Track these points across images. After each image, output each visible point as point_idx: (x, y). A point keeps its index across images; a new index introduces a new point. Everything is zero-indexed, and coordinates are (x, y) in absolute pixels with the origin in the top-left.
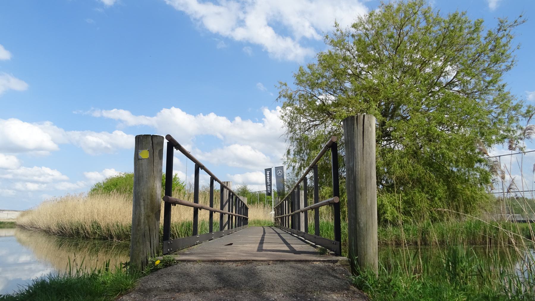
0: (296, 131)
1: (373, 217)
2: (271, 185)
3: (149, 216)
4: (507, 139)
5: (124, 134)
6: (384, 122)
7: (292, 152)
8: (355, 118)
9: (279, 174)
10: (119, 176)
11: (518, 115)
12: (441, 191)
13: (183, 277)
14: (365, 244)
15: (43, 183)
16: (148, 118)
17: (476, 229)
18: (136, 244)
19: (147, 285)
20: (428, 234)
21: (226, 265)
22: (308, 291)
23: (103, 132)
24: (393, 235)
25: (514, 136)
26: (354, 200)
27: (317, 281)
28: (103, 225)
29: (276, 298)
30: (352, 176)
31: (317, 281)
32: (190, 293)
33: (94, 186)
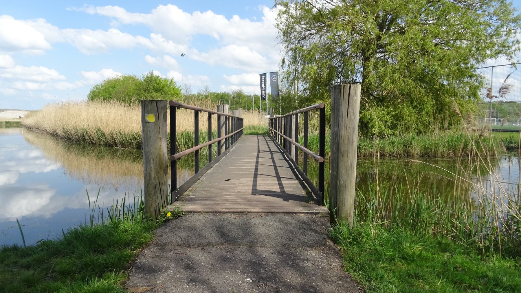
0: (291, 40)
1: (352, 176)
2: (265, 90)
3: (158, 172)
4: (501, 54)
5: (119, 32)
6: (380, 36)
7: (287, 63)
8: (342, 87)
9: (273, 80)
10: (116, 78)
11: (516, 28)
12: (429, 105)
13: (191, 231)
14: (344, 198)
15: (42, 82)
16: (143, 15)
17: (458, 142)
18: (149, 195)
19: (163, 239)
20: (412, 147)
21: (226, 216)
22: (293, 248)
23: (98, 30)
24: (379, 147)
25: (509, 51)
26: (336, 160)
27: (300, 237)
28: (106, 132)
29: (266, 255)
30: (336, 139)
31: (300, 237)
32: (198, 248)
33: (93, 88)
